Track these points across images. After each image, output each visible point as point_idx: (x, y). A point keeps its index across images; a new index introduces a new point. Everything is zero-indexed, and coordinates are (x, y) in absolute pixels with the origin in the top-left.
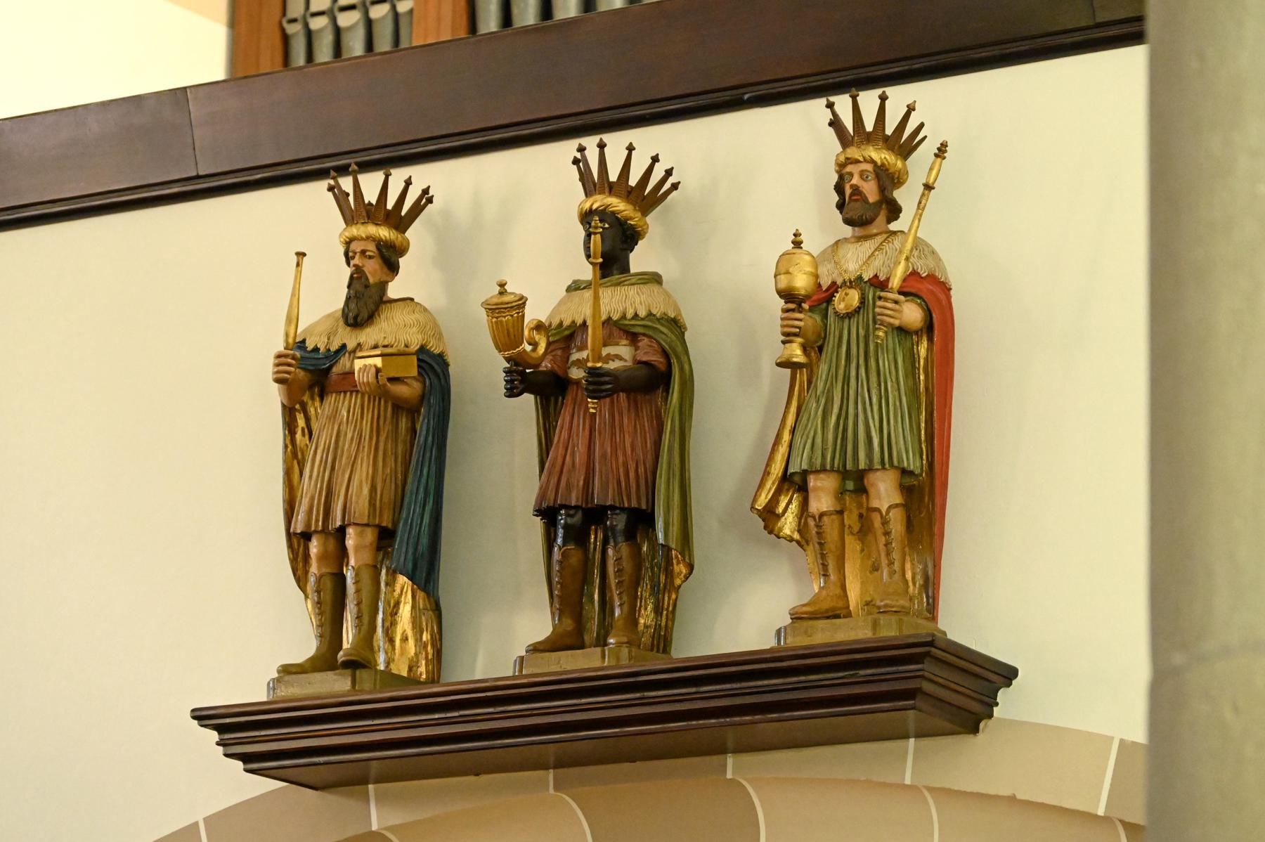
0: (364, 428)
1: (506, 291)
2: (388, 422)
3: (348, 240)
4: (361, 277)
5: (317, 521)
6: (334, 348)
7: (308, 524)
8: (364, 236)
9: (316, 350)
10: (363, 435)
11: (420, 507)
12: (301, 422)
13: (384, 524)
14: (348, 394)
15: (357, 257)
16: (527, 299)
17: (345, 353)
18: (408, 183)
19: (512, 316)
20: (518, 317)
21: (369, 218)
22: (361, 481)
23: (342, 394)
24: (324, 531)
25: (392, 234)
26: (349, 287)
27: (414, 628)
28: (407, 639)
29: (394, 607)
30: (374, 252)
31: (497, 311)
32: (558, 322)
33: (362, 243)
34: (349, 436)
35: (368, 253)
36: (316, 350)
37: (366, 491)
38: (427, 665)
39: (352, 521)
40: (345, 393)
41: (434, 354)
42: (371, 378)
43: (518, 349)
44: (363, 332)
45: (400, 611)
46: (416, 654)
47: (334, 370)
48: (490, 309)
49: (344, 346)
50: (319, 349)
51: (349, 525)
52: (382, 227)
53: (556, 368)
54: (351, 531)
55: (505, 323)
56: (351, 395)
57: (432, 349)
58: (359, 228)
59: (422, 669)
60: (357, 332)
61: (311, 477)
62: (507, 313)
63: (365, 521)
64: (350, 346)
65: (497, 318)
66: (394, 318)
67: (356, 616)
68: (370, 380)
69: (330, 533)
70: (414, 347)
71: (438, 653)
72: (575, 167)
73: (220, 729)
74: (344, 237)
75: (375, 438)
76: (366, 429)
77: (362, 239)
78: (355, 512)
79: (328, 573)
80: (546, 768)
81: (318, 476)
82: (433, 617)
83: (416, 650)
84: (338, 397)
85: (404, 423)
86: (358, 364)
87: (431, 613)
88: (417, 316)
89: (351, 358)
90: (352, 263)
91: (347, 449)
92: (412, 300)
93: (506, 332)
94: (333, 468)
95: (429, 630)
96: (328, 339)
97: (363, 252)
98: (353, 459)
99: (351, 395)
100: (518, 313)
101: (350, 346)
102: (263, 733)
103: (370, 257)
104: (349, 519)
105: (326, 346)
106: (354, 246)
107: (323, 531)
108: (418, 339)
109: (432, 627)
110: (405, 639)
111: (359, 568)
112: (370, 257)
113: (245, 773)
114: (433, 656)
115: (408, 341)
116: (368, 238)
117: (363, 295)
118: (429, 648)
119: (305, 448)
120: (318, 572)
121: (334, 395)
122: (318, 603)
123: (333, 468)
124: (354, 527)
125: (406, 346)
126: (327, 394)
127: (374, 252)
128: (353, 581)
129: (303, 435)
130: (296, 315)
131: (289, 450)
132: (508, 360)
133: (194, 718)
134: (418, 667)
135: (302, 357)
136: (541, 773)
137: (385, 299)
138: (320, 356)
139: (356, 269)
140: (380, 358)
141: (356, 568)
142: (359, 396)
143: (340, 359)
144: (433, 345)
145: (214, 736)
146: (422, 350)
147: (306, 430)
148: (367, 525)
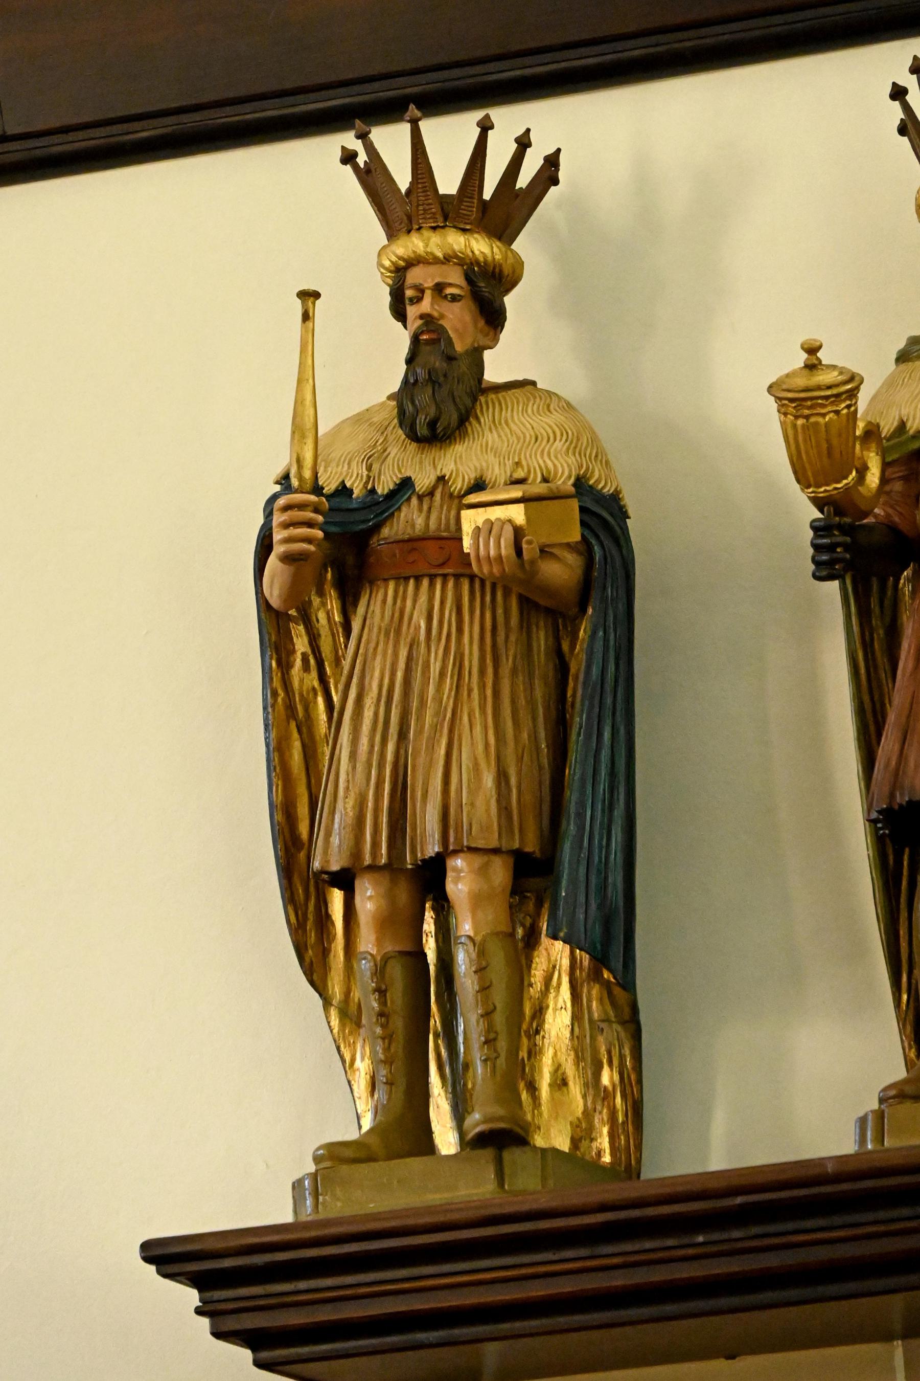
0: (467, 652)
1: (820, 361)
2: (513, 638)
3: (402, 263)
4: (440, 340)
5: (375, 844)
6: (383, 489)
7: (356, 853)
8: (440, 255)
9: (343, 491)
10: (467, 663)
11: (603, 810)
12: (301, 644)
13: (528, 849)
14: (425, 582)
15: (428, 295)
16: (862, 382)
17: (409, 499)
18: (523, 143)
19: (837, 412)
20: (848, 414)
21: (446, 218)
22: (476, 759)
23: (412, 582)
24: (393, 868)
25: (495, 250)
26: (409, 361)
27: (579, 1059)
28: (564, 1083)
29: (533, 1017)
30: (462, 288)
31: (809, 403)
32: (896, 424)
33: (432, 269)
34: (435, 668)
35: (449, 291)
36: (343, 491)
37: (488, 780)
38: (612, 1136)
39: (465, 844)
40: (418, 579)
41: (603, 496)
42: (506, 549)
43: (845, 482)
44: (448, 455)
45: (547, 1026)
46: (585, 1112)
47: (386, 532)
48: (792, 400)
49: (406, 484)
50: (351, 492)
51: (456, 852)
52: (476, 236)
53: (896, 519)
54: (458, 863)
55: (823, 429)
56: (432, 585)
57: (600, 486)
58: (429, 239)
59: (604, 1142)
60: (434, 452)
61: (353, 755)
62: (830, 408)
63: (494, 843)
64: (422, 482)
65: (807, 417)
66: (510, 421)
67: (483, 1039)
68: (503, 552)
69: (404, 870)
70: (564, 482)
71: (636, 1109)
72: (897, 104)
73: (198, 1281)
74: (394, 259)
75: (490, 671)
76: (471, 653)
77: (436, 261)
78: (470, 825)
79: (400, 952)
80: (888, 1337)
81: (371, 752)
82: (623, 1034)
83: (585, 1105)
84: (401, 589)
85: (541, 640)
86: (471, 520)
87: (616, 1026)
88: (556, 418)
89: (425, 507)
90: (412, 311)
91: (434, 699)
92: (534, 383)
93: (825, 446)
94: (403, 735)
95: (616, 1062)
96: (369, 468)
97: (439, 288)
98: (449, 715)
99: (432, 585)
100: (848, 407)
101: (422, 482)
102: (302, 1285)
103: (455, 298)
104: (458, 839)
105: (367, 483)
106: (415, 276)
107: (388, 866)
108: (569, 466)
109: (622, 1057)
110: (560, 1083)
111: (484, 941)
112: (455, 298)
113: (255, 1369)
114: (626, 1115)
115: (549, 473)
116: (447, 259)
117: (445, 376)
118: (618, 1100)
119: (311, 695)
120: (378, 951)
121: (391, 585)
122: (381, 1014)
123: (403, 735)
124: (469, 855)
125: (545, 480)
126: (372, 583)
127: (462, 288)
128: (473, 969)
129: (306, 667)
130: (312, 420)
131: (280, 700)
132: (819, 503)
133: (148, 1259)
134: (592, 1140)
135: (330, 509)
136: (876, 1348)
137: (483, 386)
138: (354, 505)
139: (426, 324)
140: (522, 505)
141: (478, 939)
142: (451, 584)
143: (399, 509)
144: (600, 475)
145: (192, 1297)
146: (581, 485)
147: (312, 661)
148: (496, 851)
